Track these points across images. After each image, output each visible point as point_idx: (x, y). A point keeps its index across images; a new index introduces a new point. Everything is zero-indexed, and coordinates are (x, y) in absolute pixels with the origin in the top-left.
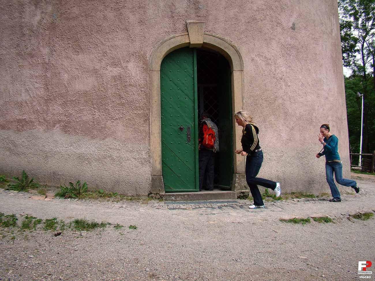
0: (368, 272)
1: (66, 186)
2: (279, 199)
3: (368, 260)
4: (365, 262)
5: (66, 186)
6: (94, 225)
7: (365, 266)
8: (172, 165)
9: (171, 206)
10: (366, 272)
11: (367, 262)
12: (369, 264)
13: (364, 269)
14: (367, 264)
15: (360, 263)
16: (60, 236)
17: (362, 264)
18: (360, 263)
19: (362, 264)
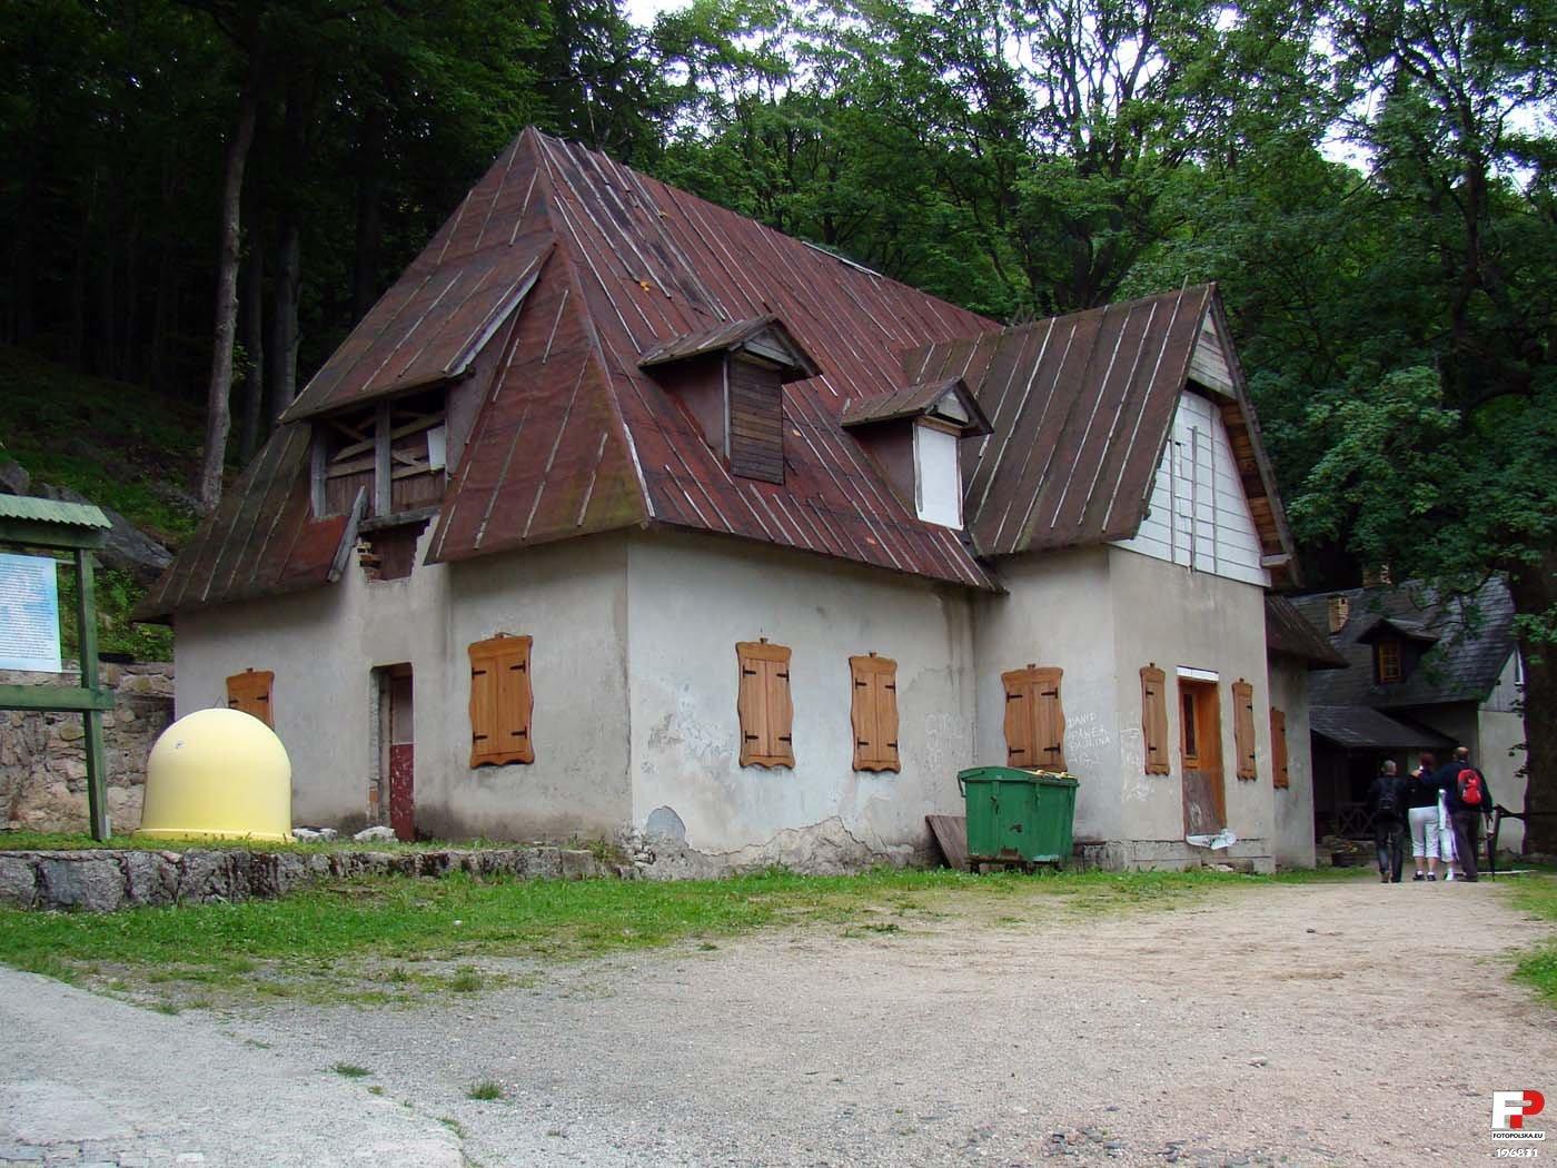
0: (1529, 1133)
1: (1193, 554)
2: (117, 510)
3: (1532, 1086)
4: (1519, 1096)
5: (1193, 554)
6: (550, 257)
7: (1518, 1111)
8: (1505, 1104)
9: (246, 1030)
10: (1521, 1133)
11: (1528, 1095)
12: (1535, 1101)
13: (1515, 1122)
14: (1529, 1103)
15: (1500, 1098)
16: (360, 1086)
17: (1509, 1104)
18: (1500, 1098)
19: (1509, 1104)
